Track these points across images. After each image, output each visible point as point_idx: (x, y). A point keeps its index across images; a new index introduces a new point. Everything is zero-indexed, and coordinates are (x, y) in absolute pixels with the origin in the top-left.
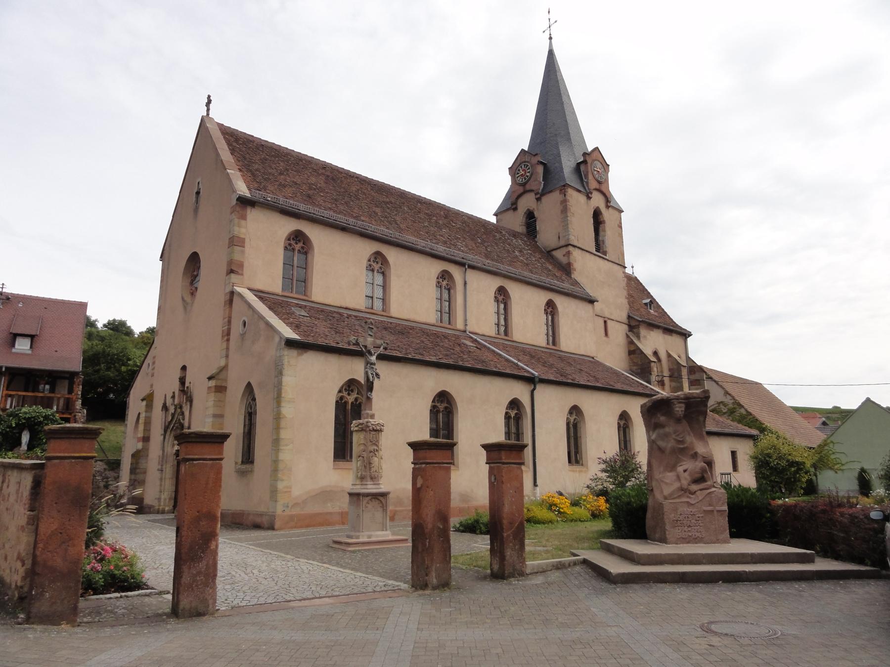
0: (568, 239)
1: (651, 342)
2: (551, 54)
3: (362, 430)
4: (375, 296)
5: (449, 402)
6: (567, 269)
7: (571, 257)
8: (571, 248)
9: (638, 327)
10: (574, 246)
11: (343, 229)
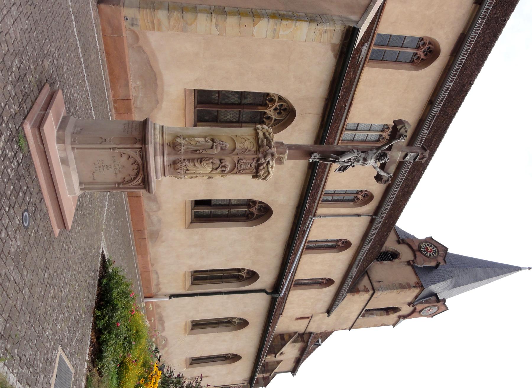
0: (378, 290)
1: (290, 351)
2: (518, 269)
3: (259, 146)
4: (357, 133)
5: (258, 217)
6: (354, 289)
7: (364, 293)
8: (371, 292)
9: (303, 341)
11: (431, 103)
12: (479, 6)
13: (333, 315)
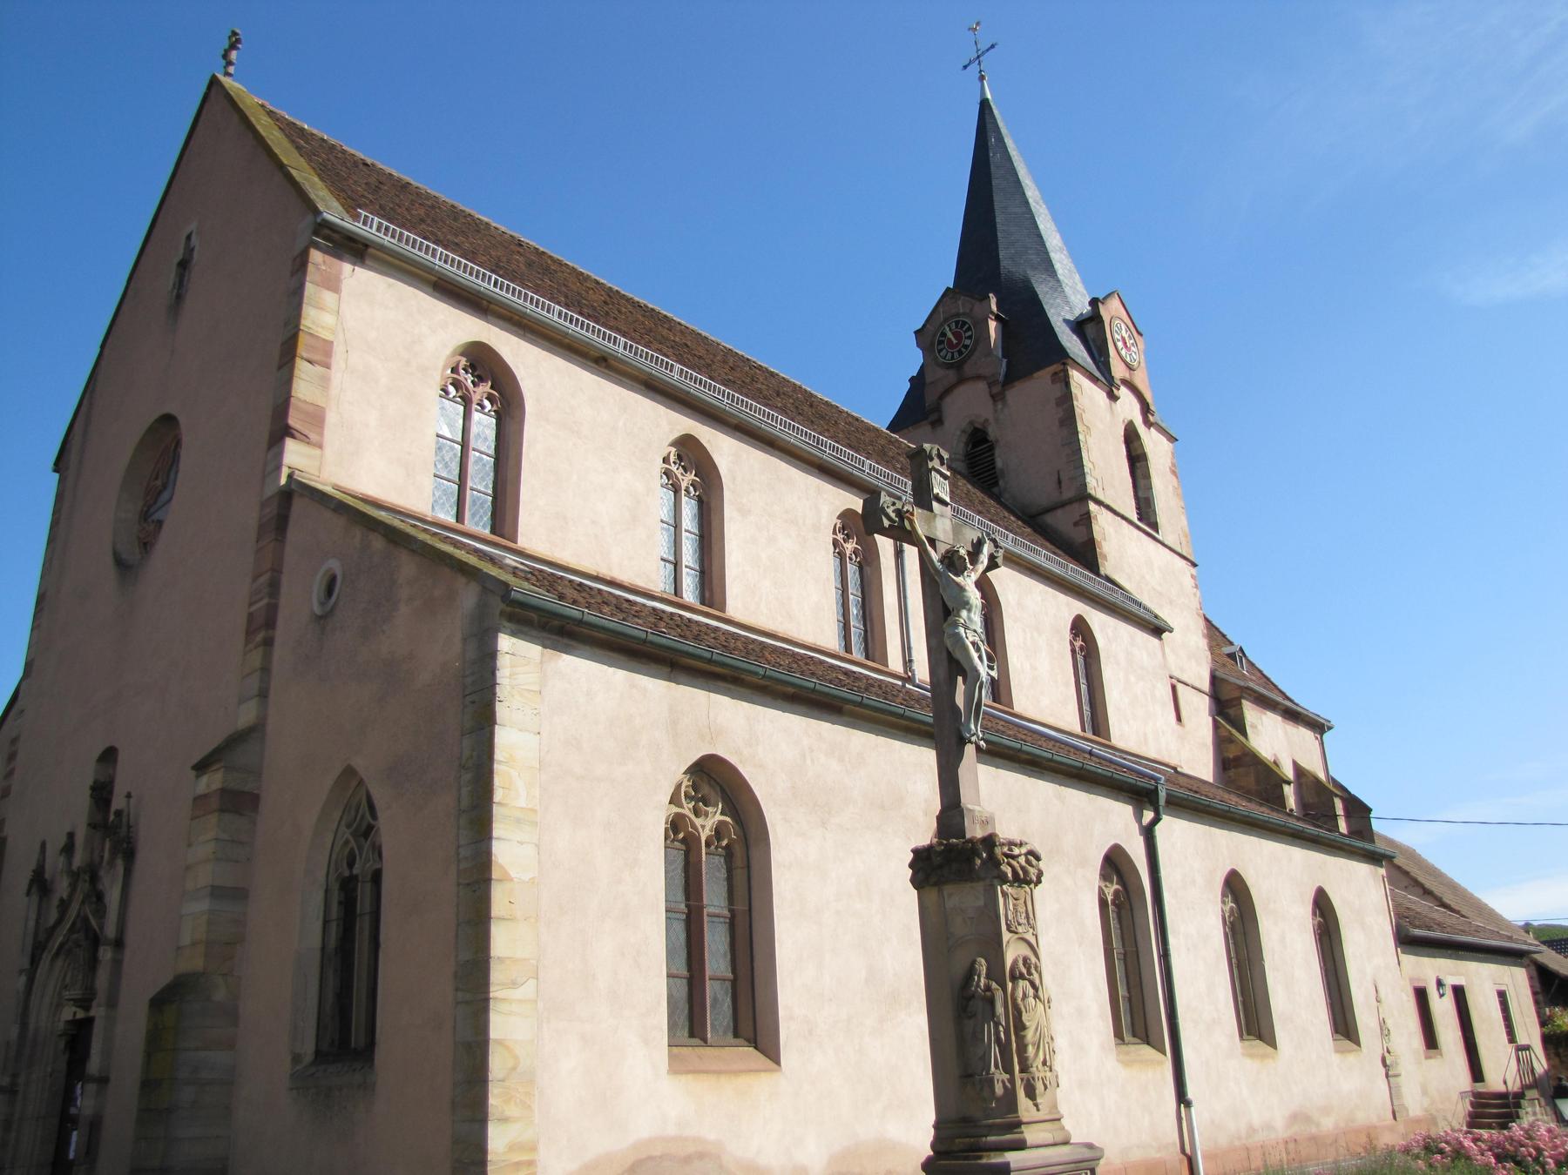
1: (1270, 737)
6: (1085, 553)
10: (1099, 502)
11: (601, 363)
12: (371, 250)
13: (1166, 614)
